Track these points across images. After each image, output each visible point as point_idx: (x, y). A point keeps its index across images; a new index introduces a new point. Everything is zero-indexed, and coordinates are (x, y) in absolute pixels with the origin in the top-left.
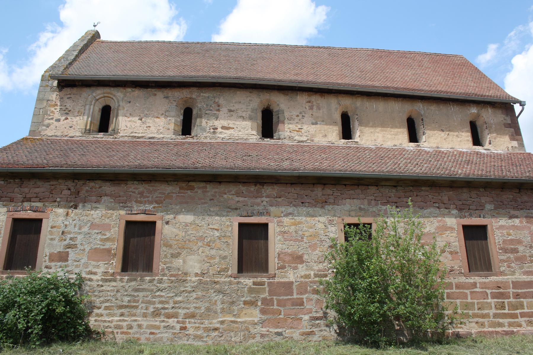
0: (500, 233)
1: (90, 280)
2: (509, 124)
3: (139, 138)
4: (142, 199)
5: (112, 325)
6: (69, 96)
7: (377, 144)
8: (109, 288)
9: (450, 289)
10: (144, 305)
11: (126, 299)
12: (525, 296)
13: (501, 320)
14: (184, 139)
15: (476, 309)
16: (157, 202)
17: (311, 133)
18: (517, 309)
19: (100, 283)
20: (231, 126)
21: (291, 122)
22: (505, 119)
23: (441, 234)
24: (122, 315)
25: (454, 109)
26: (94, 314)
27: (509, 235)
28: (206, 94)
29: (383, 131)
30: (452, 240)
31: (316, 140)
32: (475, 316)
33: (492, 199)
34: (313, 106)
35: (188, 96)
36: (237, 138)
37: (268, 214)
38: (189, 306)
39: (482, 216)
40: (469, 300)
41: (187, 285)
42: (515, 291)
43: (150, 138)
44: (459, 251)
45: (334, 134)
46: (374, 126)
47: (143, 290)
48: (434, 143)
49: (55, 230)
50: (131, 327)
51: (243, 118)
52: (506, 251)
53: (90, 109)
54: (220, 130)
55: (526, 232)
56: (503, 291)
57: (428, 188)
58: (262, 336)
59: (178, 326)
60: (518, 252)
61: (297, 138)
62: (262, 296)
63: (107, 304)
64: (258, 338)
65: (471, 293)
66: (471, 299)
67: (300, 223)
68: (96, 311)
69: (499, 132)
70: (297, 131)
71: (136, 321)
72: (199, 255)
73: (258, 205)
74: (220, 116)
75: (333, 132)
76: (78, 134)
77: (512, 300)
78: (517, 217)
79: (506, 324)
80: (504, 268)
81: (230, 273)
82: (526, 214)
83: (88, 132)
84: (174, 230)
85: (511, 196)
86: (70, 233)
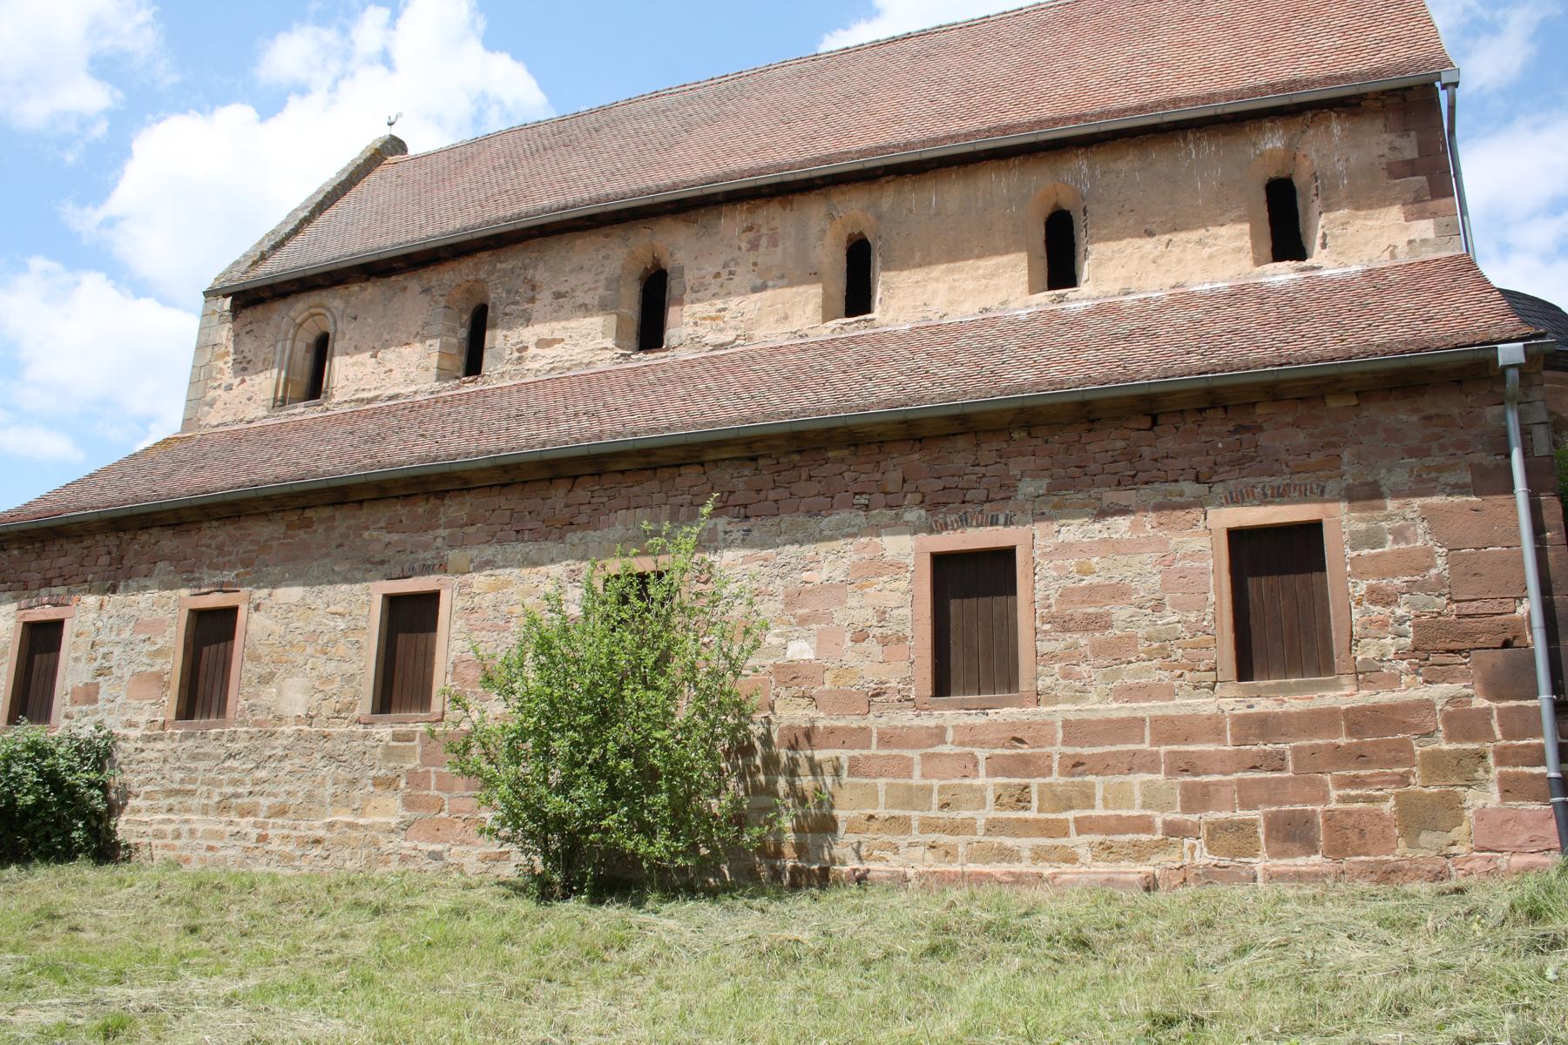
0: (1056, 568)
1: (125, 739)
2: (1410, 163)
3: (370, 401)
4: (222, 560)
5: (150, 830)
6: (248, 328)
7: (930, 315)
8: (152, 755)
9: (862, 748)
10: (204, 788)
11: (178, 776)
12: (1104, 766)
13: (1009, 842)
14: (458, 387)
15: (935, 806)
16: (245, 566)
17: (746, 317)
18: (1070, 808)
19: (140, 744)
20: (557, 335)
21: (698, 295)
22: (1393, 149)
23: (861, 587)
24: (170, 810)
25: (1199, 154)
26: (128, 808)
27: (1085, 571)
28: (509, 262)
29: (952, 271)
30: (893, 600)
31: (759, 333)
32: (928, 826)
33: (1047, 461)
34: (758, 239)
35: (471, 277)
36: (567, 364)
37: (443, 568)
38: (276, 790)
39: (1002, 519)
40: (917, 780)
41: (276, 743)
42: (1070, 750)
43: (391, 398)
44: (908, 633)
45: (810, 308)
46: (927, 261)
47: (206, 756)
48: (1116, 279)
49: (82, 639)
50: (178, 836)
51: (585, 309)
52: (1064, 625)
53: (283, 350)
54: (532, 350)
55: (1149, 557)
56: (1029, 751)
57: (846, 452)
58: (404, 859)
59: (254, 833)
60: (1109, 626)
61: (712, 338)
62: (409, 766)
63: (149, 788)
64: (394, 866)
65: (926, 758)
66: (923, 776)
67: (507, 584)
68: (132, 802)
69: (1364, 198)
70: (713, 319)
71: (186, 821)
72: (305, 675)
73: (426, 547)
74: (535, 315)
75: (806, 303)
76: (262, 412)
77: (1056, 778)
78: (1124, 511)
79: (1026, 853)
80: (1048, 681)
81: (357, 713)
82: (1160, 499)
83: (281, 402)
84: (268, 622)
85: (1120, 444)
86: (103, 644)
